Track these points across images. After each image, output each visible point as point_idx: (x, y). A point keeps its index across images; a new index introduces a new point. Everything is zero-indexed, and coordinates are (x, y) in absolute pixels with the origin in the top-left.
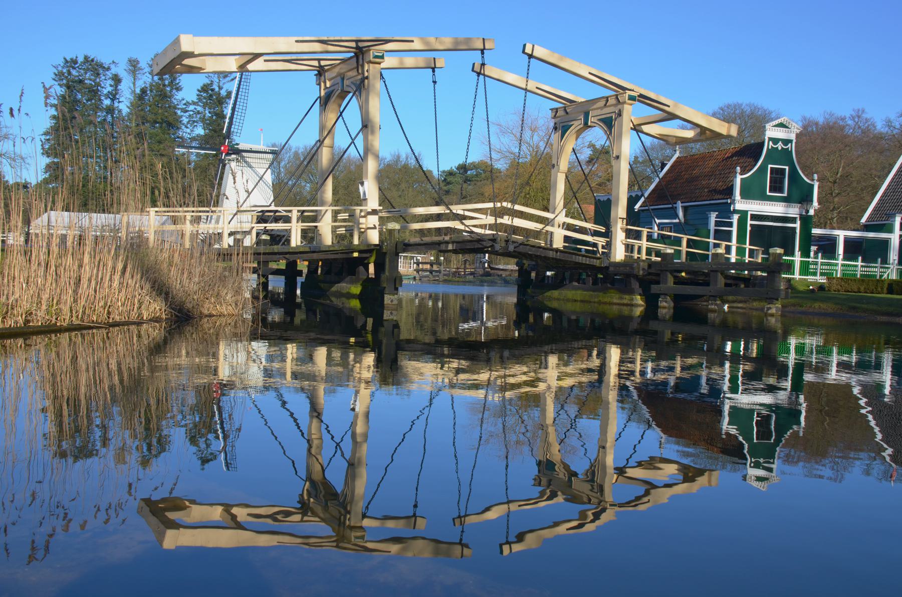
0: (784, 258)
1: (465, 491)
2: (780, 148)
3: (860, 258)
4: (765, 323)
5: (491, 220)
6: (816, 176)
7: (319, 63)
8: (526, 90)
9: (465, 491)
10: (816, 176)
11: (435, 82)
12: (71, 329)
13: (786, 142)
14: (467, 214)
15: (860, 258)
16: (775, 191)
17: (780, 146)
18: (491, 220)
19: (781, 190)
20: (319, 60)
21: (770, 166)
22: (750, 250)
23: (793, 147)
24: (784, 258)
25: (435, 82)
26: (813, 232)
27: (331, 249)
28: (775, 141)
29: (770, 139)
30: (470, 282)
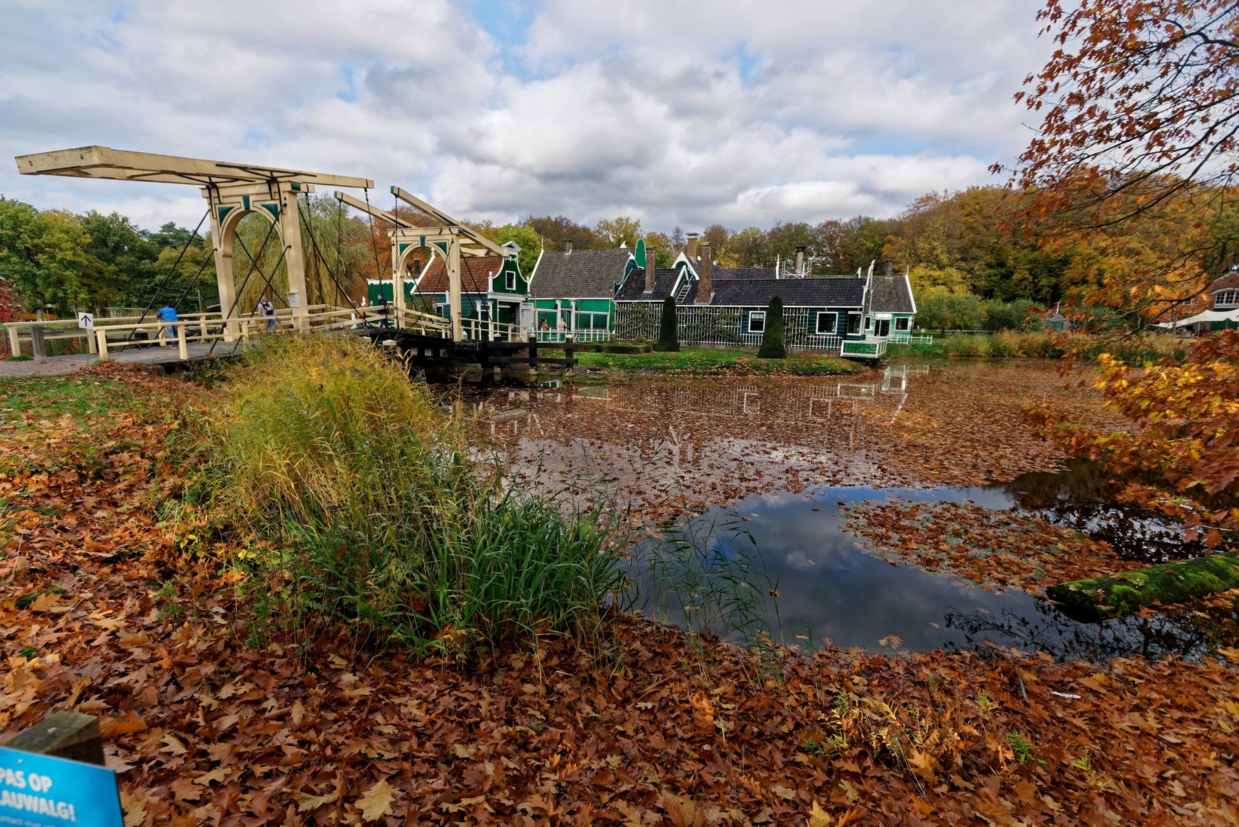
13: (513, 257)
17: (510, 259)
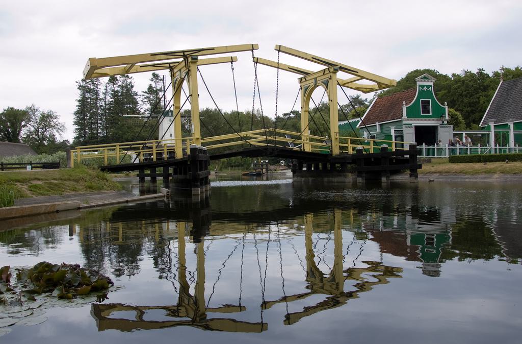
0: (417, 147)
1: (263, 277)
2: (425, 90)
3: (424, 144)
4: (206, 238)
5: (263, 138)
6: (446, 103)
7: (170, 65)
8: (278, 68)
9: (263, 277)
10: (446, 103)
11: (233, 69)
12: (45, 213)
13: (428, 86)
14: (252, 136)
15: (424, 144)
16: (425, 113)
17: (425, 89)
18: (263, 138)
19: (428, 112)
20: (169, 63)
21: (421, 100)
22: (426, 148)
23: (432, 89)
24: (417, 147)
25: (233, 69)
26: (150, 171)
27: (225, 152)
28: (423, 86)
29: (420, 86)
30: (124, 194)
